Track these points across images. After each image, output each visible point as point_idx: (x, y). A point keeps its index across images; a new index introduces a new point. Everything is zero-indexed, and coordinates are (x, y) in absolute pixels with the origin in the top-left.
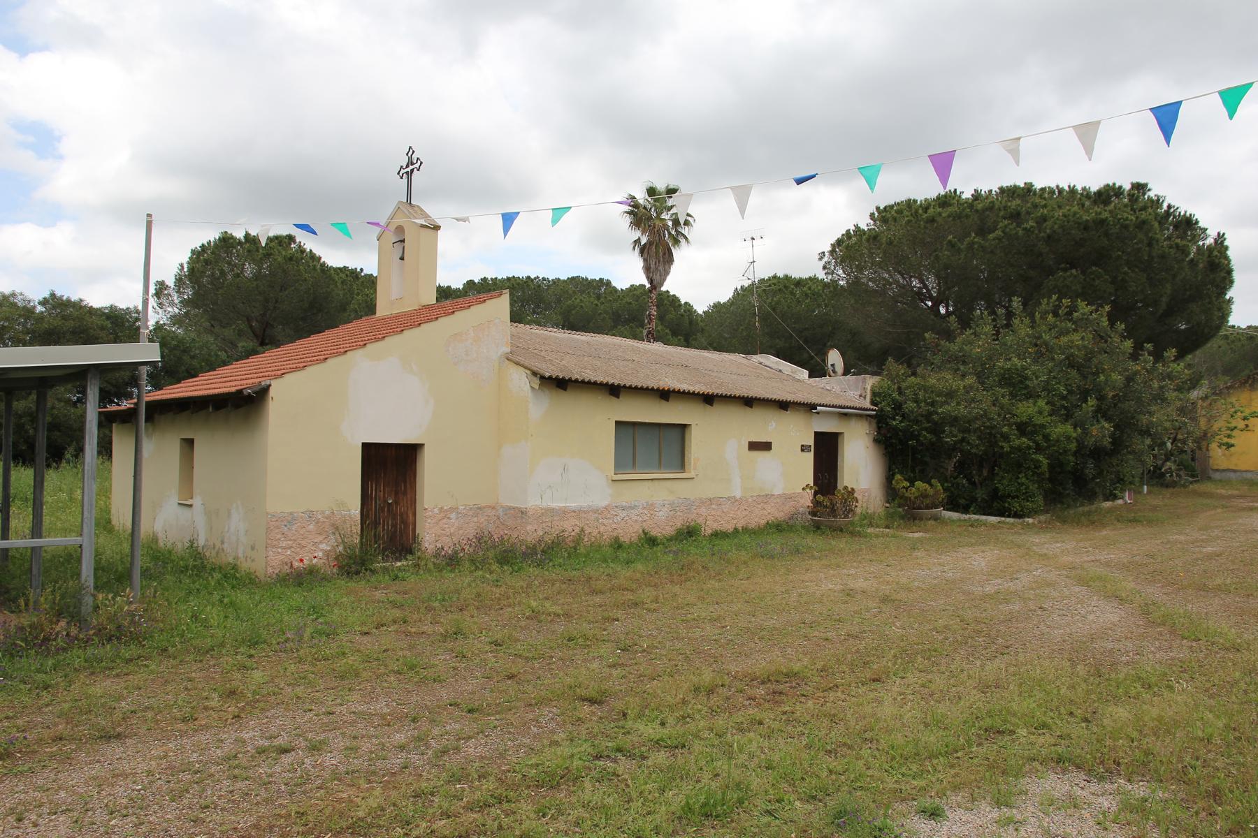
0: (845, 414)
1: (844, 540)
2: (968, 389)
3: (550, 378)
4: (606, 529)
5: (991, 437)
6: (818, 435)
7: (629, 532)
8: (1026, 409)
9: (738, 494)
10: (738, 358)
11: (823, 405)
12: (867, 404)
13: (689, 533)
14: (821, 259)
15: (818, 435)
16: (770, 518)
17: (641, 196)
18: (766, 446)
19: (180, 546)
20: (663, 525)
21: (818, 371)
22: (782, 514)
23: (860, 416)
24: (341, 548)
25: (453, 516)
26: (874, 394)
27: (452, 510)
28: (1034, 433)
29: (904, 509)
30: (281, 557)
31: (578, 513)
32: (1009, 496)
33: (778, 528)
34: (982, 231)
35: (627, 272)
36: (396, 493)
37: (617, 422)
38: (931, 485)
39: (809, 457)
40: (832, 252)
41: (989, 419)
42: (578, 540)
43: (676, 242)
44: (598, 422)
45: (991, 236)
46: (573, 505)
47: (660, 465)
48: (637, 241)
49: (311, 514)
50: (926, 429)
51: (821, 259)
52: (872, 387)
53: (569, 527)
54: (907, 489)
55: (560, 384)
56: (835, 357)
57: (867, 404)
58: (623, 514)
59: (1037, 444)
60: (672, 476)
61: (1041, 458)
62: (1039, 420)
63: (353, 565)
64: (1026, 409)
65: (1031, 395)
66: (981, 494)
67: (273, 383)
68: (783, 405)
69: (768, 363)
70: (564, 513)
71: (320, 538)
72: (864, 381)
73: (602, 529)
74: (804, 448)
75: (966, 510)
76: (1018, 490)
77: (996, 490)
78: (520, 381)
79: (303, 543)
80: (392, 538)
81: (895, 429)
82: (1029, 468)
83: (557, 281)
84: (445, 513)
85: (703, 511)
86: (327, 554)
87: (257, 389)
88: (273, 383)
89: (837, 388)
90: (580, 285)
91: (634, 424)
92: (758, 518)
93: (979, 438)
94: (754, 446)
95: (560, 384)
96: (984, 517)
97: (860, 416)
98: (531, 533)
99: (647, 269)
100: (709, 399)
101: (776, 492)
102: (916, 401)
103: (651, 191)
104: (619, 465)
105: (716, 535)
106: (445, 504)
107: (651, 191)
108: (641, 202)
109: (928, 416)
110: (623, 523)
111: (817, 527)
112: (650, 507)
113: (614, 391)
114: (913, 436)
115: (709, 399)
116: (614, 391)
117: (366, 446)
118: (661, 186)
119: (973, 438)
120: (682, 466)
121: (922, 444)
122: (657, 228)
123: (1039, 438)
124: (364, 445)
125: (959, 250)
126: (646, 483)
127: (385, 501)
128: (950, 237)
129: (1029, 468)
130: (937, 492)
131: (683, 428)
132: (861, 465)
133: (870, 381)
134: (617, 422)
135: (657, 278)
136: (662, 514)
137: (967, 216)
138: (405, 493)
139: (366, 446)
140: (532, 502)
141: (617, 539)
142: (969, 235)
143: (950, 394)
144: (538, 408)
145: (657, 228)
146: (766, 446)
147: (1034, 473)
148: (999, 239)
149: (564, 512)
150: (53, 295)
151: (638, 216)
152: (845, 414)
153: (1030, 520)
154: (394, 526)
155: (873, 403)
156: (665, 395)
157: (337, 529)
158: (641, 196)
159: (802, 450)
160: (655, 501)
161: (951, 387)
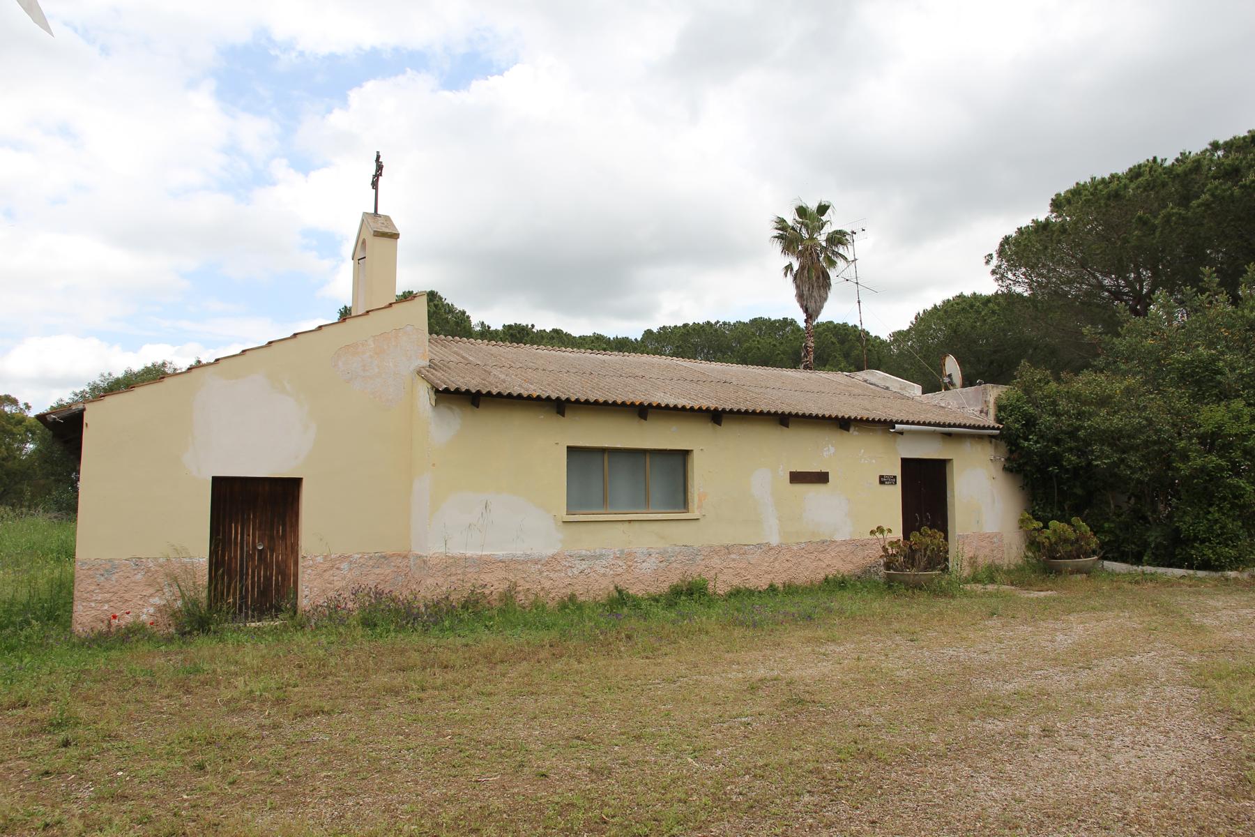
0: (951, 434)
2: (1128, 391)
3: (447, 391)
4: (555, 585)
5: (1163, 455)
6: (906, 462)
8: (1212, 415)
9: (774, 540)
10: (840, 377)
11: (902, 423)
12: (990, 421)
13: (690, 593)
14: (987, 262)
15: (906, 462)
16: (831, 573)
17: (791, 218)
18: (822, 478)
19: (521, 596)
21: (933, 384)
22: (850, 567)
23: (981, 437)
24: (179, 603)
25: (345, 566)
26: (1000, 408)
27: (343, 558)
28: (1227, 447)
29: (1046, 561)
30: (94, 613)
31: (507, 564)
32: (1196, 538)
33: (838, 584)
34: (1185, 201)
35: (779, 301)
36: (272, 538)
37: (571, 450)
38: (1069, 523)
39: (895, 492)
40: (1001, 252)
41: (1157, 431)
42: (508, 597)
43: (832, 263)
44: (545, 448)
45: (1194, 203)
46: (500, 553)
47: (644, 502)
48: (789, 268)
49: (138, 562)
50: (1070, 450)
51: (987, 262)
52: (998, 399)
53: (495, 583)
54: (1038, 530)
55: (474, 399)
56: (952, 366)
57: (990, 421)
58: (584, 565)
59: (1234, 464)
61: (1242, 483)
62: (1233, 429)
63: (195, 623)
64: (1212, 415)
65: (1224, 395)
66: (1154, 536)
67: (88, 406)
68: (844, 424)
69: (873, 380)
70: (484, 563)
71: (151, 591)
72: (985, 392)
73: (547, 584)
74: (883, 480)
75: (1137, 559)
76: (1210, 530)
77: (1177, 530)
78: (424, 396)
79: (127, 596)
80: (265, 592)
81: (1029, 453)
82: (1224, 499)
83: (739, 324)
84: (333, 564)
85: (716, 561)
86: (159, 609)
87: (65, 414)
88: (88, 406)
89: (953, 405)
90: (759, 324)
91: (603, 451)
92: (809, 571)
93: (1145, 458)
94: (796, 478)
95: (474, 399)
96: (1161, 570)
97: (981, 437)
98: (429, 588)
99: (801, 297)
100: (716, 416)
101: (839, 538)
102: (1056, 413)
103: (802, 211)
104: (572, 506)
105: (736, 593)
106: (330, 548)
107: (802, 211)
108: (790, 222)
109: (1072, 434)
111: (890, 583)
112: (628, 557)
113: (560, 406)
114: (1057, 459)
115: (716, 416)
116: (560, 406)
117: (217, 481)
118: (813, 206)
119: (1133, 458)
120: (685, 504)
121: (1067, 471)
122: (811, 249)
123: (1237, 455)
124: (215, 479)
125: (1154, 228)
126: (619, 526)
127: (254, 547)
128: (1140, 213)
129: (1224, 499)
130: (1083, 536)
131: (685, 454)
132: (983, 503)
133: (994, 392)
134: (571, 450)
135: (812, 306)
136: (649, 565)
137: (1164, 185)
138: (284, 537)
139: (217, 481)
140: (433, 548)
141: (572, 598)
142: (1165, 206)
143: (1104, 401)
144: (442, 430)
145: (811, 249)
146: (822, 478)
147: (1233, 506)
148: (1207, 205)
151: (788, 238)
152: (949, 435)
153: (1232, 574)
154: (268, 579)
155: (999, 420)
156: (643, 411)
157: (176, 579)
158: (791, 218)
159: (882, 482)
160: (635, 548)
161: (1108, 396)
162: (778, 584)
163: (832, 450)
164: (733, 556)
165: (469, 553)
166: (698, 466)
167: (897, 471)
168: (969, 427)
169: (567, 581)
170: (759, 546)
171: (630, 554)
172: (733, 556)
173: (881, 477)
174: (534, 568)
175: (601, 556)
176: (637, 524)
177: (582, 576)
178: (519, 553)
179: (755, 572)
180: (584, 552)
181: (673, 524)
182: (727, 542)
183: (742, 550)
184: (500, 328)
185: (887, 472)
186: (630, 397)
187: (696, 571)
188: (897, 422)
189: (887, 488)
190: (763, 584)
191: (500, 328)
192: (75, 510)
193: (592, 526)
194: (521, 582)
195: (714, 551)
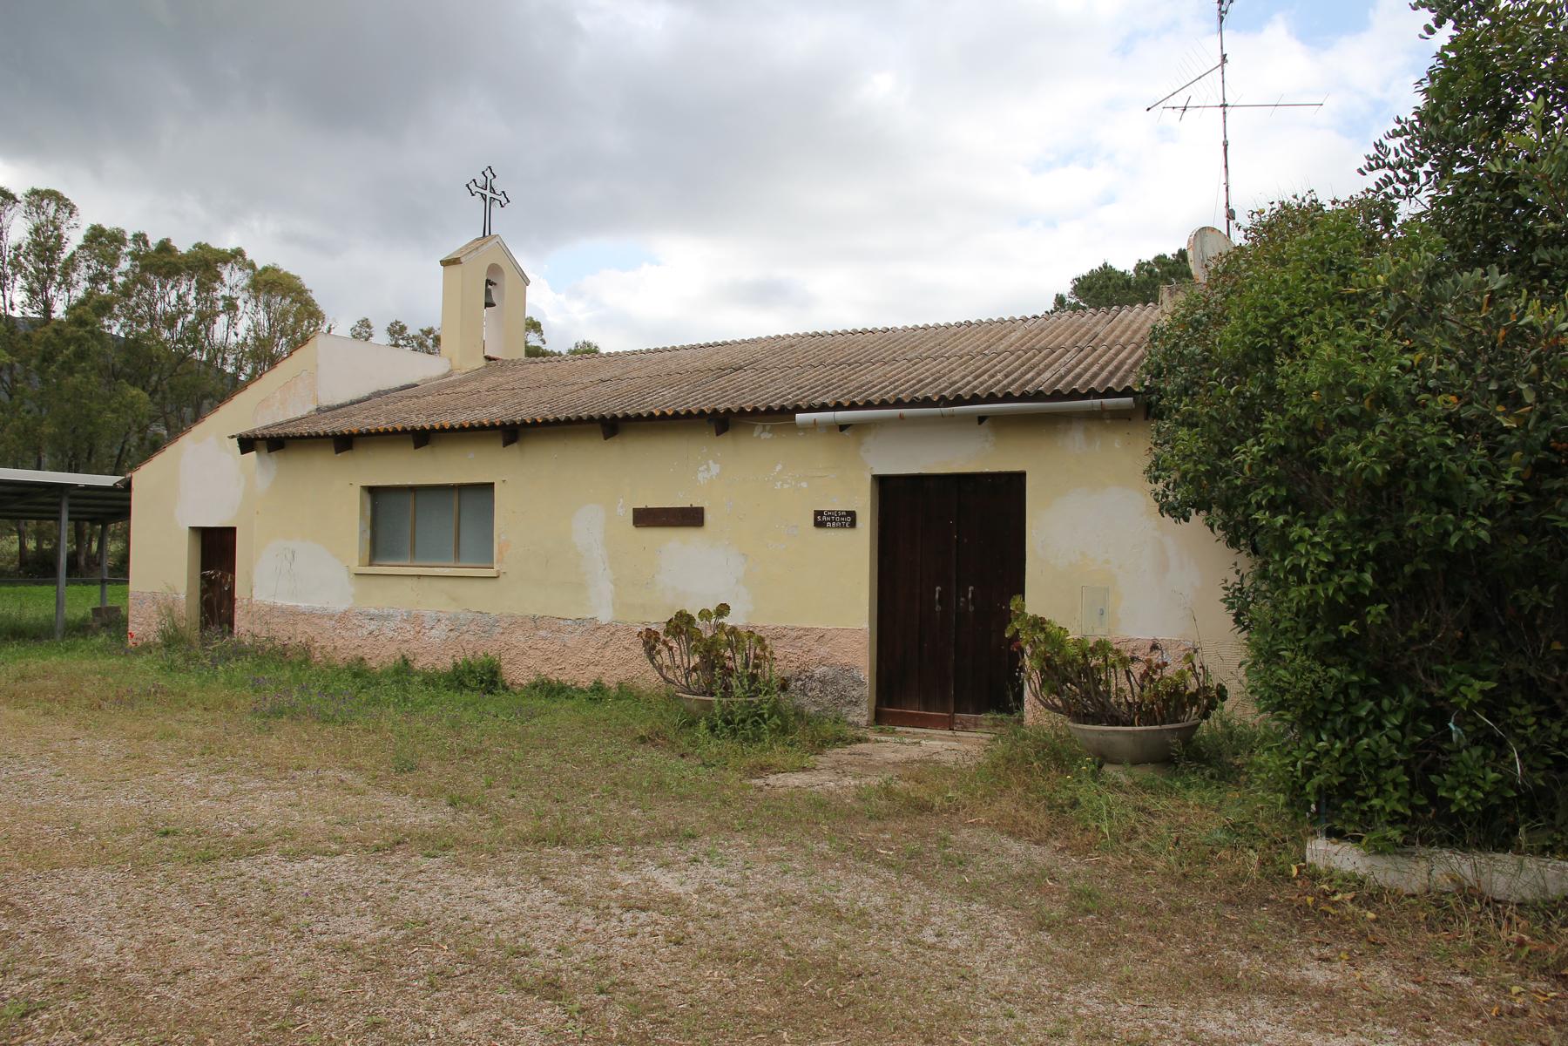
1: (1193, 798)
4: (344, 645)
6: (886, 486)
7: (382, 656)
9: (605, 616)
13: (481, 678)
15: (886, 486)
18: (691, 517)
20: (437, 651)
46: (303, 605)
53: (300, 634)
58: (372, 626)
60: (446, 572)
73: (339, 643)
85: (518, 638)
94: (646, 518)
100: (511, 433)
106: (261, 583)
110: (371, 640)
112: (415, 619)
113: (344, 443)
115: (511, 433)
120: (486, 557)
126: (408, 581)
131: (489, 487)
134: (372, 491)
136: (438, 634)
146: (691, 517)
149: (293, 614)
150: (1105, 266)
152: (843, 427)
156: (422, 438)
160: (426, 611)
162: (610, 681)
163: (715, 468)
164: (542, 633)
165: (280, 602)
166: (502, 499)
167: (862, 502)
168: (1025, 397)
169: (357, 642)
170: (580, 621)
171: (417, 617)
172: (542, 633)
173: (818, 513)
174: (329, 624)
175: (387, 618)
176: (427, 580)
177: (371, 640)
178: (318, 606)
179: (574, 660)
180: (372, 611)
181: (477, 583)
182: (532, 611)
183: (554, 624)
184: (1420, 100)
185: (835, 503)
186: (483, 416)
187: (489, 648)
188: (798, 409)
189: (834, 537)
190: (585, 680)
191: (1420, 100)
192: (127, 574)
193: (381, 581)
194: (318, 638)
195: (515, 623)
